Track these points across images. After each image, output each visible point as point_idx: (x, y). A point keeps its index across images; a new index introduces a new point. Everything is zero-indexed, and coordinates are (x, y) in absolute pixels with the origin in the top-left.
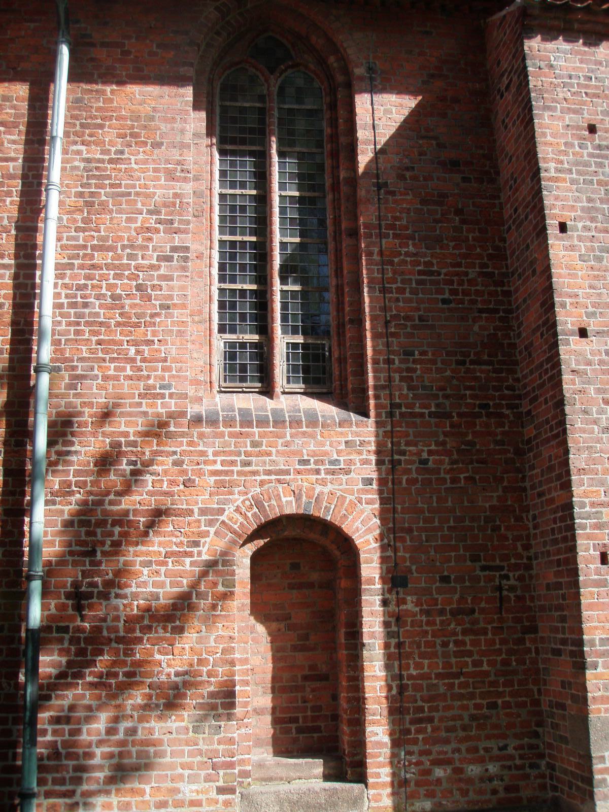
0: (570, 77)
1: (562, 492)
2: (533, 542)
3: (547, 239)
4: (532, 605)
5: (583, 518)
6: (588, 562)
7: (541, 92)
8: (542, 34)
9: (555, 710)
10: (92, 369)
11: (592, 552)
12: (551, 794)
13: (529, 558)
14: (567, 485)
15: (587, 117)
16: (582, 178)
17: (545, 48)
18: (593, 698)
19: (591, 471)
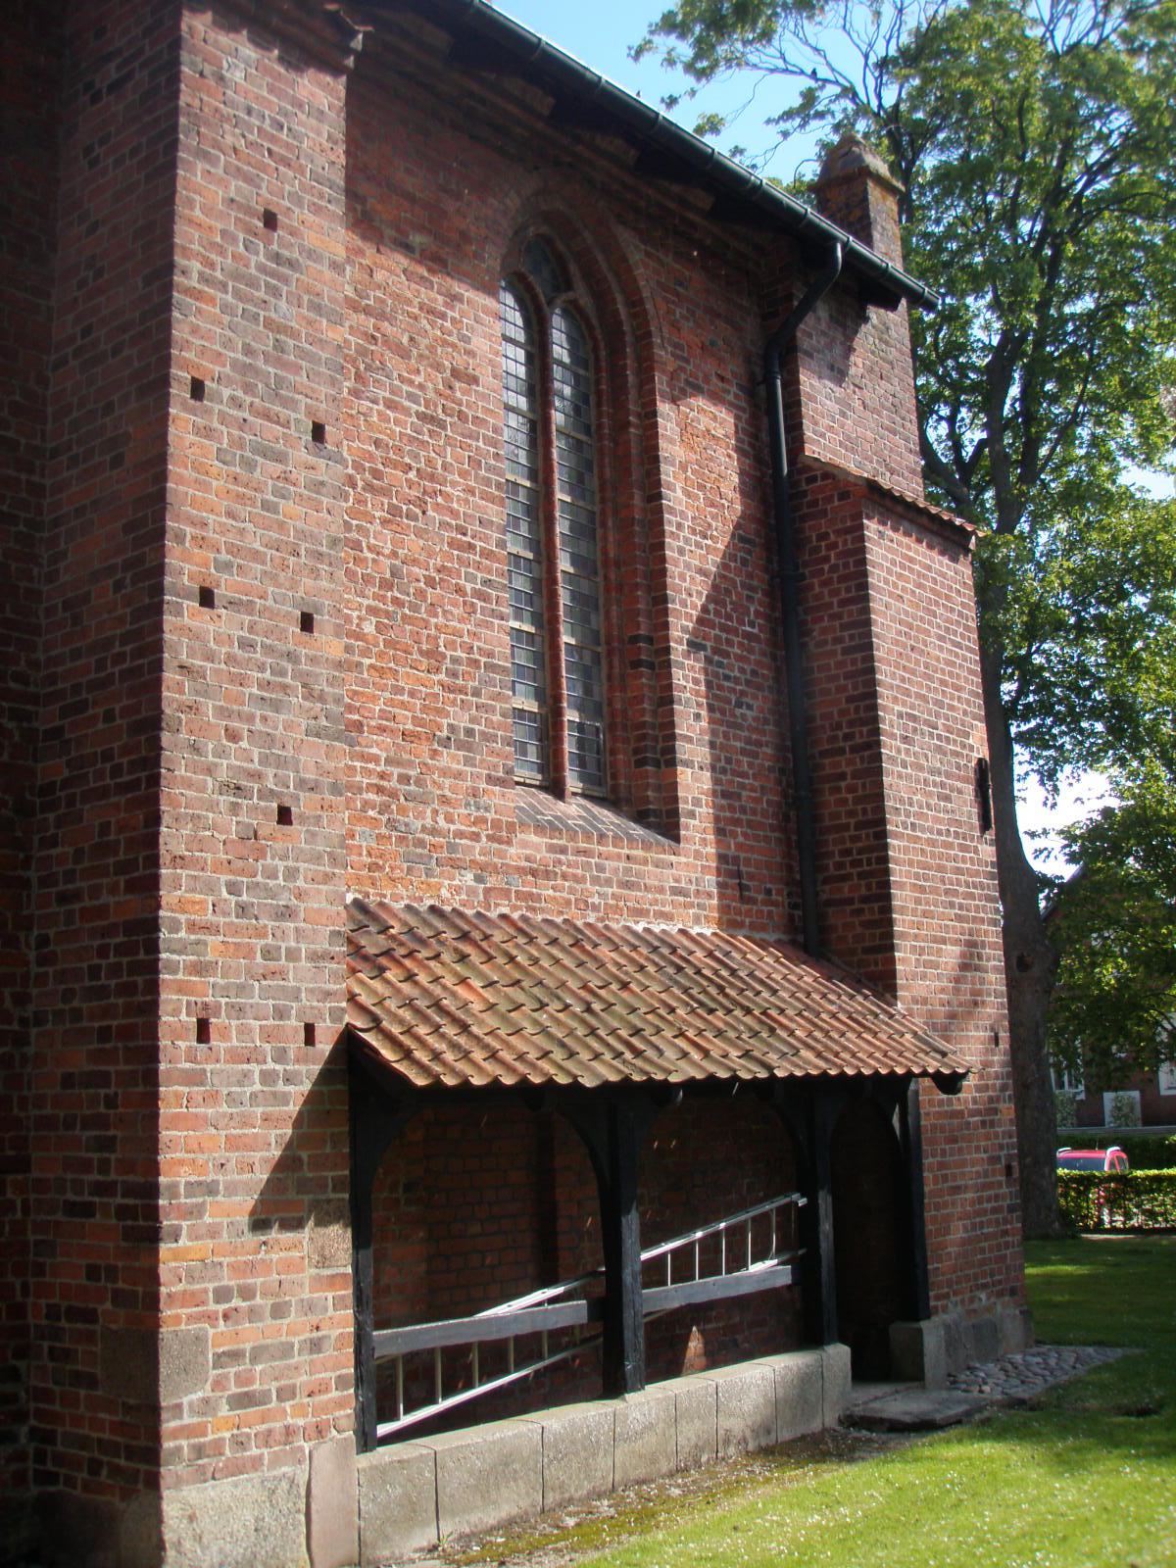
0: (249, 112)
1: (128, 897)
2: (34, 992)
3: (167, 404)
4: (22, 1115)
5: (173, 952)
6: (177, 1035)
7: (197, 120)
8: (215, 12)
9: (64, 1323)
10: (852, 637)
11: (183, 1017)
12: (34, 1490)
13: (24, 1022)
14: (149, 885)
15: (266, 195)
16: (241, 306)
17: (216, 41)
18: (169, 1295)
19: (195, 863)
